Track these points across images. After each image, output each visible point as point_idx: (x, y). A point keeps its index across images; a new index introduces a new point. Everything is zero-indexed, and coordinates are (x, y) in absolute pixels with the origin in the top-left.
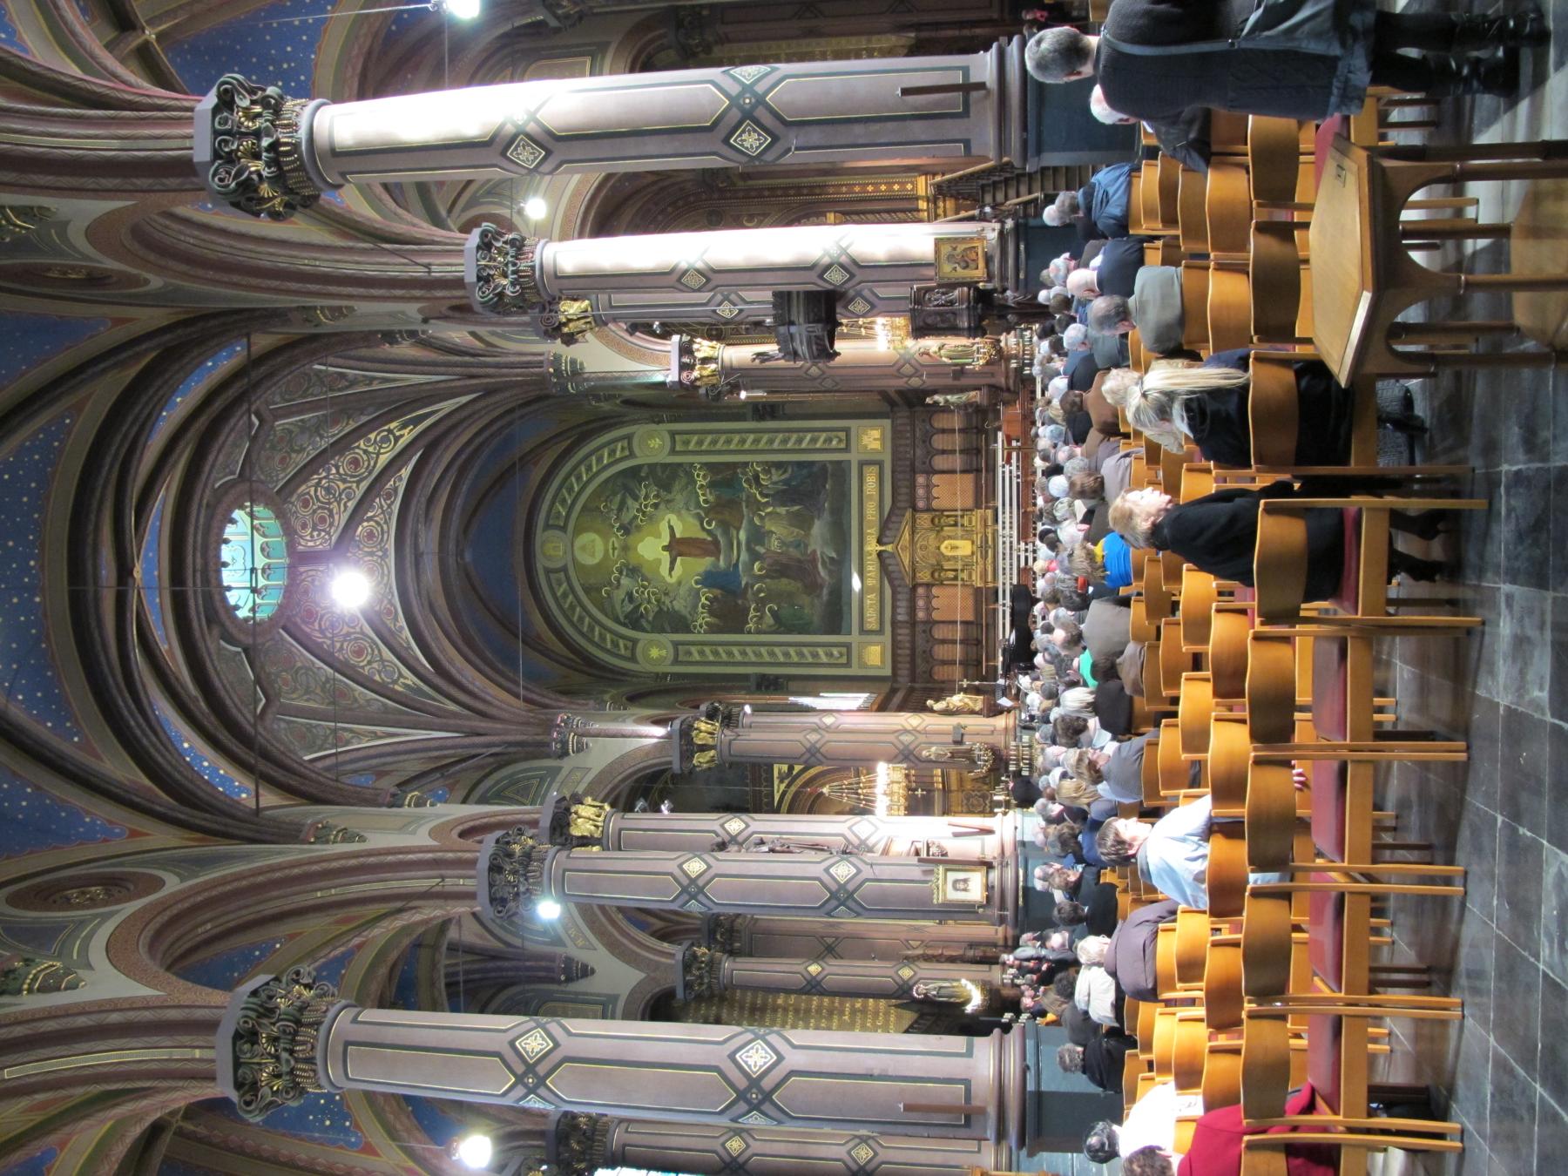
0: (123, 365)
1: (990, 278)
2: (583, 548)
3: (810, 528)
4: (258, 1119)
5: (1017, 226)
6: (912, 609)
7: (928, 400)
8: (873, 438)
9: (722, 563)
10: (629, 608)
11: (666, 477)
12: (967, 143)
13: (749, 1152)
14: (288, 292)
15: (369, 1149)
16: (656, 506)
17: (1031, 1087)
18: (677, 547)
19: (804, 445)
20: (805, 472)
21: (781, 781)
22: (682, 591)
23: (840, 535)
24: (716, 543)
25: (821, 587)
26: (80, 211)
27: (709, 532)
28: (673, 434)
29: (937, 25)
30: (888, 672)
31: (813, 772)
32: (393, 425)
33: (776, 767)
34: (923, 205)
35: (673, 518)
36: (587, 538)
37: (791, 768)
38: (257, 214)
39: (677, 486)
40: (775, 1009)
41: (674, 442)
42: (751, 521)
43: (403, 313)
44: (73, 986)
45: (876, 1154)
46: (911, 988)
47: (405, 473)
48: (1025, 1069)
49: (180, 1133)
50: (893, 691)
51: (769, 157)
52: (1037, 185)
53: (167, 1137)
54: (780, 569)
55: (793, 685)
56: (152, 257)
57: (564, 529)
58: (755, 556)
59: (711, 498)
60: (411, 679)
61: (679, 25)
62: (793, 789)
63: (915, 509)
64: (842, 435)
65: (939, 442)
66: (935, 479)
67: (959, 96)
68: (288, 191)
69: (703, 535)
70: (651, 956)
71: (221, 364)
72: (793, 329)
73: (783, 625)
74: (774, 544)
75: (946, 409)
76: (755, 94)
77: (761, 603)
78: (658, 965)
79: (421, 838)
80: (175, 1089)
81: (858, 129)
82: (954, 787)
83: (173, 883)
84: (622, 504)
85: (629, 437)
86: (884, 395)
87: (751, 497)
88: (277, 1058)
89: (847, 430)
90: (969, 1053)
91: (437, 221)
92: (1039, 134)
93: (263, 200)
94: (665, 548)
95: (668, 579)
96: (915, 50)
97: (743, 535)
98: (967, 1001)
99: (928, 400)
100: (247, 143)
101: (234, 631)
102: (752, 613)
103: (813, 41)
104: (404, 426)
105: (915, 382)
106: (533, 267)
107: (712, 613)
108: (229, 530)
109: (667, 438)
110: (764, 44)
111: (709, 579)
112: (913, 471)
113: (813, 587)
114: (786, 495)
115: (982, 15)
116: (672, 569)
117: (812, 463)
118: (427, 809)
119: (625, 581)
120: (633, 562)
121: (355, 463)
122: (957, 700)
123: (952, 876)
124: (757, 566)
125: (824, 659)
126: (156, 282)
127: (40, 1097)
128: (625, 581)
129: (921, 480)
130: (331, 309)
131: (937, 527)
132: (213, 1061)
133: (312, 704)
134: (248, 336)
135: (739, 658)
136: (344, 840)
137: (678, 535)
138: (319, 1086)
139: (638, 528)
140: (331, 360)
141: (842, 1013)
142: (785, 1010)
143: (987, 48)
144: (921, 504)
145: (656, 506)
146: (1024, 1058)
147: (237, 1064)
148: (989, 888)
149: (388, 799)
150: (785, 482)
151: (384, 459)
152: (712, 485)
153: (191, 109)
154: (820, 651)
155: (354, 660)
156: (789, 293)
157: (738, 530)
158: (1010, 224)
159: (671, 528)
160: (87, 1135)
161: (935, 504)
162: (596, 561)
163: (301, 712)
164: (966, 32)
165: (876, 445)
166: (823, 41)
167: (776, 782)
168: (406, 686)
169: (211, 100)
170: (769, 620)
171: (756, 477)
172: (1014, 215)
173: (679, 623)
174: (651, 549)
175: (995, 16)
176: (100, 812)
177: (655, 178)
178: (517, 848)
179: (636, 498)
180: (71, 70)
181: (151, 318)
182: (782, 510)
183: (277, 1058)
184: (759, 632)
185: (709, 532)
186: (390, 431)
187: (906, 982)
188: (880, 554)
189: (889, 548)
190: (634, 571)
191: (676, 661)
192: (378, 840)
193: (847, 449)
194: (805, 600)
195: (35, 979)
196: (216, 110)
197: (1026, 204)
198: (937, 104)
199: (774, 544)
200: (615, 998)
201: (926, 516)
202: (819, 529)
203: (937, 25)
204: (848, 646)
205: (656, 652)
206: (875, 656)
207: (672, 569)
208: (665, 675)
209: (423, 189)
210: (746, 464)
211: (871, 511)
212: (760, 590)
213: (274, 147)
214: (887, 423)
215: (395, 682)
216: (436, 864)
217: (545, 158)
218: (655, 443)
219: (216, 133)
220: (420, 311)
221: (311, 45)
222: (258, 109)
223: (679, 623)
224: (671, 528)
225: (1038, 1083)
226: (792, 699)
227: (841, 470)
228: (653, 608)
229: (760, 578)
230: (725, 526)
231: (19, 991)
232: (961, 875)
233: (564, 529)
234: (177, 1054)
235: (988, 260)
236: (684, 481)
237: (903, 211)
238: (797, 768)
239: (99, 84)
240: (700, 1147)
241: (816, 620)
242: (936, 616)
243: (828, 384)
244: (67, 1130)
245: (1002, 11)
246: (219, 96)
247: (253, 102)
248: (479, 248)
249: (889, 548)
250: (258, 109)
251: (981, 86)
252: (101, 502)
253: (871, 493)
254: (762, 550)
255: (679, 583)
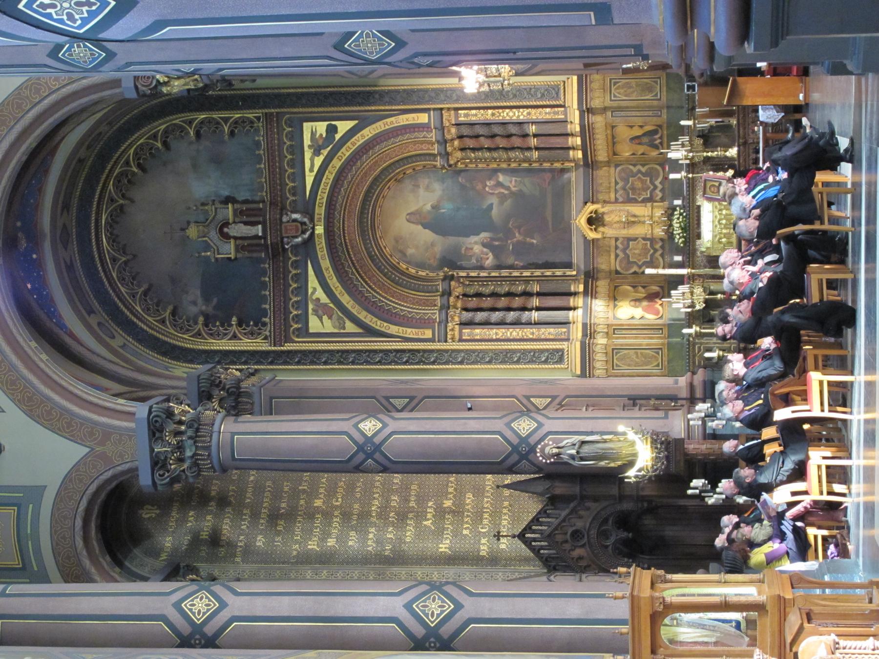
13: (224, 615)
21: (317, 153)
31: (368, 133)
33: (307, 127)
40: (310, 515)
46: (532, 450)
62: (337, 164)
70: (95, 417)
78: (107, 433)
82: (602, 155)
98: (631, 464)
141: (420, 516)
142: (328, 515)
167: (308, 154)
187: (523, 440)
200: (36, 492)
240: (136, 611)
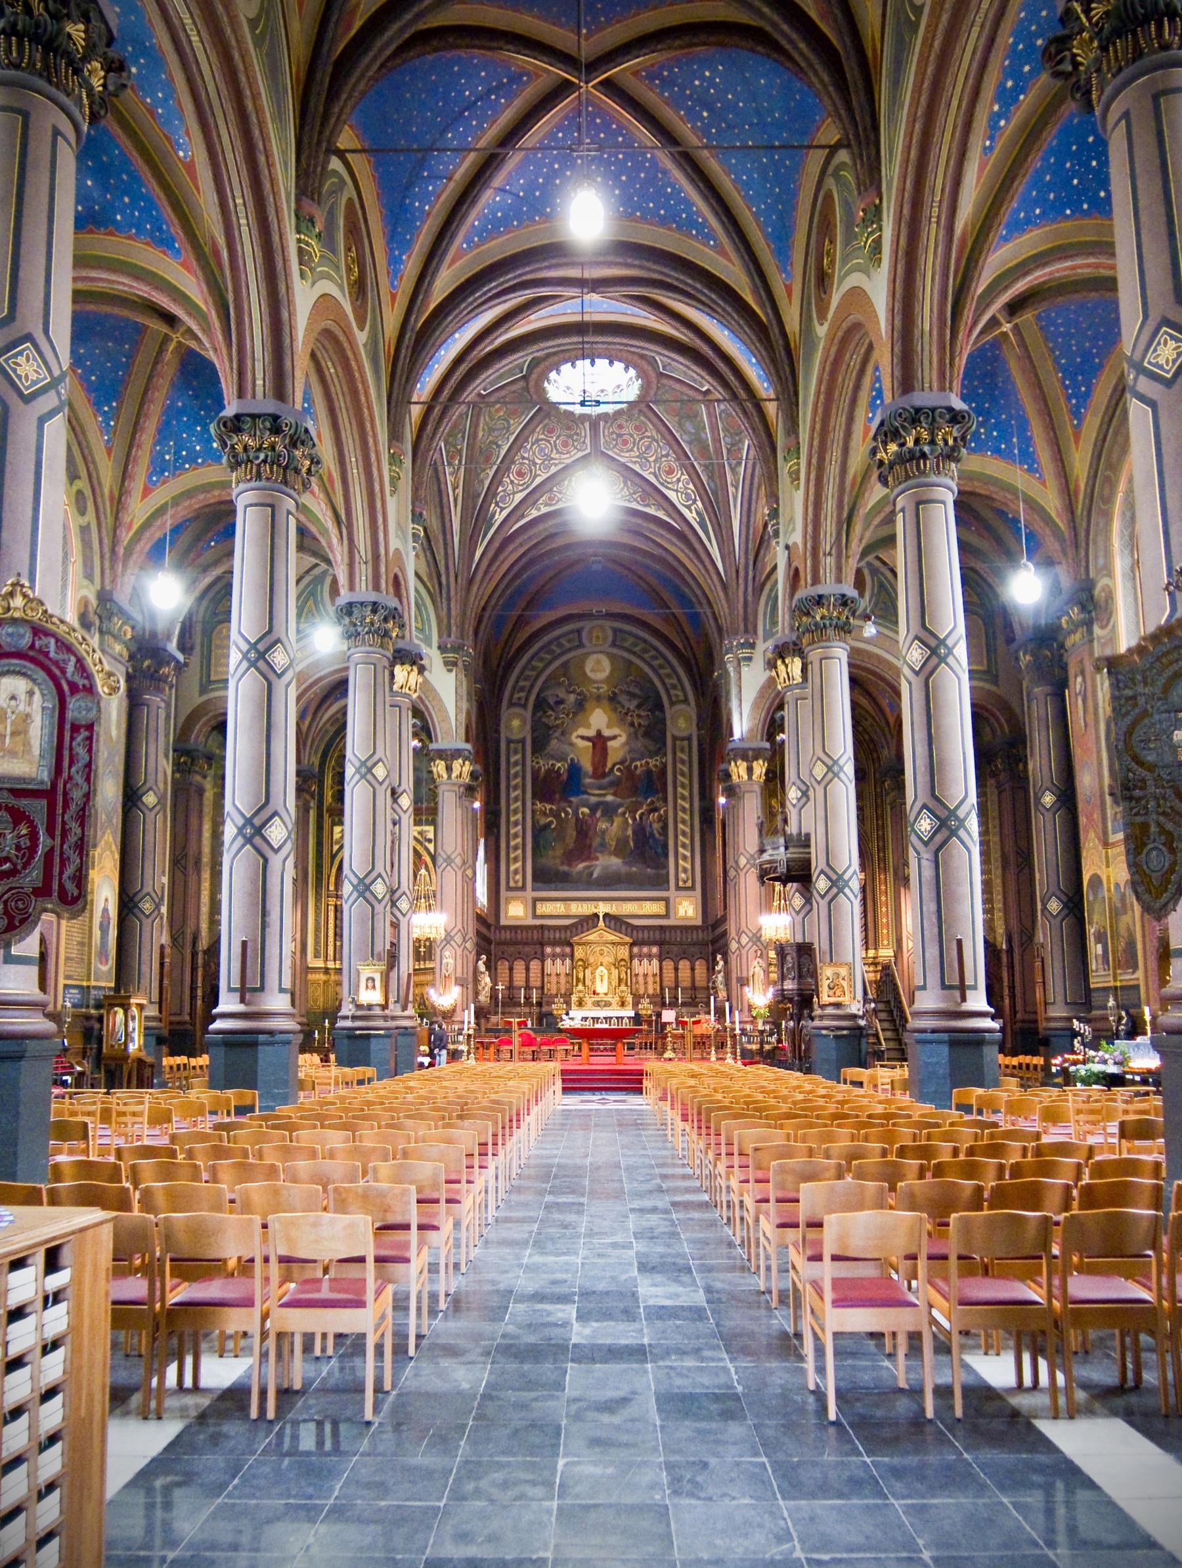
0: (755, 291)
1: (822, 1007)
2: (598, 662)
3: (616, 855)
4: (212, 431)
5: (860, 1028)
6: (554, 944)
7: (719, 957)
8: (687, 910)
9: (588, 781)
10: (551, 701)
11: (653, 732)
12: (924, 988)
14: (812, 438)
15: (146, 492)
16: (632, 724)
17: (262, 1038)
18: (599, 742)
19: (681, 850)
20: (660, 850)
22: (566, 748)
23: (609, 881)
24: (604, 775)
25: (570, 865)
26: (878, 288)
27: (612, 769)
28: (689, 739)
29: (1011, 966)
30: (503, 922)
32: (699, 503)
33: (431, 828)
34: (871, 953)
35: (623, 739)
36: (606, 664)
37: (430, 841)
38: (875, 438)
39: (647, 742)
41: (683, 739)
42: (620, 806)
43: (794, 530)
44: (302, 275)
45: (148, 917)
47: (661, 514)
48: (271, 1033)
49: (166, 339)
50: (488, 926)
51: (913, 838)
52: (892, 1045)
53: (163, 328)
54: (584, 831)
55: (492, 840)
56: (840, 334)
57: (614, 645)
58: (593, 808)
59: (638, 772)
60: (499, 517)
61: (1012, 745)
63: (632, 945)
64: (689, 884)
65: (684, 965)
66: (655, 962)
67: (957, 983)
68: (891, 466)
69: (609, 765)
71: (763, 385)
72: (782, 849)
73: (539, 832)
74: (603, 825)
75: (711, 970)
76: (958, 828)
77: (557, 815)
79: (394, 543)
80: (231, 361)
81: (933, 907)
83: (361, 337)
84: (632, 695)
85: (686, 701)
86: (724, 919)
87: (640, 805)
88: (259, 449)
89: (693, 888)
90: (281, 990)
91: (864, 554)
92: (930, 1042)
93: (885, 443)
94: (599, 733)
95: (575, 734)
96: (991, 948)
97: (610, 798)
99: (719, 957)
100: (925, 435)
101: (538, 370)
102: (548, 807)
103: (999, 864)
104: (698, 513)
105: (734, 946)
106: (828, 640)
107: (548, 771)
108: (619, 366)
109: (685, 734)
110: (997, 822)
111: (575, 770)
112: (661, 944)
113: (571, 856)
114: (641, 833)
115: (1019, 1007)
116: (583, 738)
117: (666, 856)
118: (411, 544)
119: (572, 697)
120: (587, 705)
121: (670, 472)
122: (486, 980)
123: (377, 977)
124: (586, 810)
125: (512, 868)
126: (821, 330)
127: (225, 254)
128: (572, 697)
129: (655, 950)
130: (798, 471)
131: (617, 964)
132: (254, 397)
133: (481, 434)
134: (777, 399)
135: (513, 795)
136: (392, 478)
137: (610, 744)
138: (238, 482)
139: (615, 710)
140: (752, 452)
143: (990, 1003)
144: (636, 950)
145: (632, 724)
146: (282, 1032)
147: (254, 417)
148: (370, 1007)
149: (418, 510)
150: (652, 835)
151: (672, 495)
152: (649, 772)
153: (951, 390)
154: (519, 864)
155: (514, 468)
156: (809, 846)
157: (615, 794)
158: (862, 1023)
159: (614, 738)
160: (193, 286)
161: (636, 962)
162: (588, 671)
163: (475, 425)
164: (1006, 992)
165: (681, 913)
166: (999, 871)
168: (493, 515)
169: (958, 404)
170: (543, 821)
171: (656, 810)
172: (870, 1026)
173: (539, 745)
174: (599, 719)
175: (1019, 1016)
176: (411, 266)
177: (892, 721)
178: (390, 625)
179: (639, 707)
180: (980, 287)
181: (792, 323)
182: (630, 832)
183: (259, 449)
184: (534, 812)
185: (612, 769)
186: (695, 501)
188: (596, 916)
189: (601, 923)
190: (581, 706)
191: (509, 742)
192: (391, 503)
193: (678, 888)
194: (559, 852)
195: (307, 244)
196: (950, 409)
197: (876, 1036)
198: (951, 966)
199: (603, 825)
201: (626, 955)
202: (615, 862)
203: (1011, 966)
204: (523, 888)
205: (515, 724)
206: (516, 911)
207: (583, 738)
208: (497, 731)
209: (890, 540)
210: (665, 800)
211: (629, 908)
212: (567, 813)
213: (924, 456)
214: (699, 922)
215: (497, 504)
216: (376, 557)
217: (913, 670)
218: (682, 723)
219: (933, 410)
220: (795, 544)
221: (997, 451)
222: (951, 442)
223: (539, 745)
224: (614, 738)
225: (263, 1044)
226: (482, 841)
227: (660, 882)
228: (551, 722)
229: (576, 813)
230: (616, 784)
231: (299, 232)
232: (378, 984)
233: (614, 645)
234: (259, 366)
235: (838, 1005)
236: (652, 748)
237: (866, 937)
238: (431, 847)
239: (968, 314)
241: (543, 861)
242: (549, 962)
243: (732, 873)
244: (199, 273)
245: (1023, 1021)
246: (961, 411)
247: (955, 439)
248: (843, 596)
249: (601, 923)
250: (951, 442)
251: (964, 999)
252: (649, 270)
253: (642, 908)
254: (598, 814)
255: (572, 744)
